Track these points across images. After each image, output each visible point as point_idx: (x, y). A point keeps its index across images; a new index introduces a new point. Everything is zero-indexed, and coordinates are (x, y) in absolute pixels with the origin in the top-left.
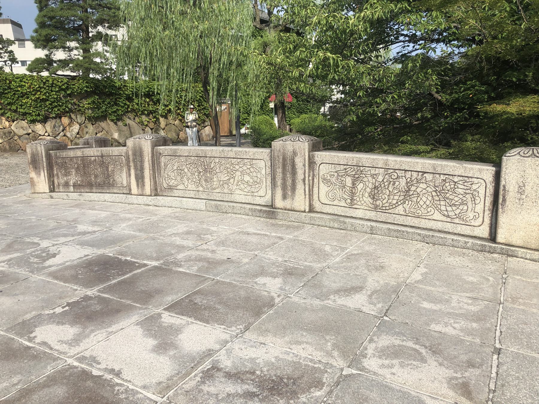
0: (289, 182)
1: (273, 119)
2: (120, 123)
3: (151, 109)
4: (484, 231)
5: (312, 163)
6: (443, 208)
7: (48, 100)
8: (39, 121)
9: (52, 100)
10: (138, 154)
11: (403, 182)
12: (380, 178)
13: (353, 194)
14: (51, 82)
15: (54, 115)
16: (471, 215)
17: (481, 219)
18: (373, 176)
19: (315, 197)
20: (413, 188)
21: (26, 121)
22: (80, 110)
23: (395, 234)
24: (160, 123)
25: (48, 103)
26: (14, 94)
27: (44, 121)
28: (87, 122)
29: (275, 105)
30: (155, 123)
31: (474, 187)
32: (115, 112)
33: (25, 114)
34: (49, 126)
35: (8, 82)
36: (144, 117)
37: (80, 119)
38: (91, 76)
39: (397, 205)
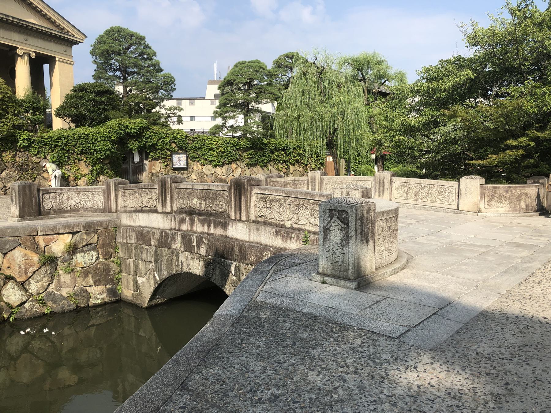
0: (381, 190)
1: (373, 167)
2: (265, 169)
3: (285, 159)
4: (456, 208)
5: (391, 182)
6: (441, 198)
7: (225, 153)
8: (218, 166)
9: (228, 152)
10: (313, 179)
11: (426, 188)
12: (418, 187)
13: (407, 194)
14: (228, 141)
15: (228, 162)
16: (451, 200)
17: (454, 202)
18: (415, 187)
19: (392, 196)
20: (430, 191)
21: (211, 165)
22: (242, 159)
23: (423, 209)
24: (289, 169)
25: (225, 154)
26: (207, 148)
27: (222, 166)
28: (246, 167)
29: (376, 157)
30: (287, 169)
31: (452, 190)
32: (263, 161)
33: (211, 161)
34: (225, 168)
35: (204, 141)
36: (279, 164)
37: (242, 165)
38: (248, 136)
39: (424, 198)
